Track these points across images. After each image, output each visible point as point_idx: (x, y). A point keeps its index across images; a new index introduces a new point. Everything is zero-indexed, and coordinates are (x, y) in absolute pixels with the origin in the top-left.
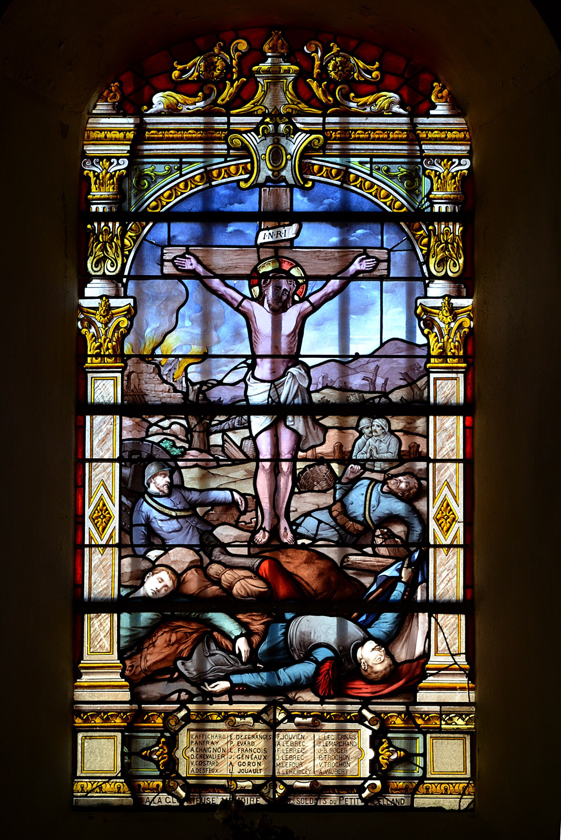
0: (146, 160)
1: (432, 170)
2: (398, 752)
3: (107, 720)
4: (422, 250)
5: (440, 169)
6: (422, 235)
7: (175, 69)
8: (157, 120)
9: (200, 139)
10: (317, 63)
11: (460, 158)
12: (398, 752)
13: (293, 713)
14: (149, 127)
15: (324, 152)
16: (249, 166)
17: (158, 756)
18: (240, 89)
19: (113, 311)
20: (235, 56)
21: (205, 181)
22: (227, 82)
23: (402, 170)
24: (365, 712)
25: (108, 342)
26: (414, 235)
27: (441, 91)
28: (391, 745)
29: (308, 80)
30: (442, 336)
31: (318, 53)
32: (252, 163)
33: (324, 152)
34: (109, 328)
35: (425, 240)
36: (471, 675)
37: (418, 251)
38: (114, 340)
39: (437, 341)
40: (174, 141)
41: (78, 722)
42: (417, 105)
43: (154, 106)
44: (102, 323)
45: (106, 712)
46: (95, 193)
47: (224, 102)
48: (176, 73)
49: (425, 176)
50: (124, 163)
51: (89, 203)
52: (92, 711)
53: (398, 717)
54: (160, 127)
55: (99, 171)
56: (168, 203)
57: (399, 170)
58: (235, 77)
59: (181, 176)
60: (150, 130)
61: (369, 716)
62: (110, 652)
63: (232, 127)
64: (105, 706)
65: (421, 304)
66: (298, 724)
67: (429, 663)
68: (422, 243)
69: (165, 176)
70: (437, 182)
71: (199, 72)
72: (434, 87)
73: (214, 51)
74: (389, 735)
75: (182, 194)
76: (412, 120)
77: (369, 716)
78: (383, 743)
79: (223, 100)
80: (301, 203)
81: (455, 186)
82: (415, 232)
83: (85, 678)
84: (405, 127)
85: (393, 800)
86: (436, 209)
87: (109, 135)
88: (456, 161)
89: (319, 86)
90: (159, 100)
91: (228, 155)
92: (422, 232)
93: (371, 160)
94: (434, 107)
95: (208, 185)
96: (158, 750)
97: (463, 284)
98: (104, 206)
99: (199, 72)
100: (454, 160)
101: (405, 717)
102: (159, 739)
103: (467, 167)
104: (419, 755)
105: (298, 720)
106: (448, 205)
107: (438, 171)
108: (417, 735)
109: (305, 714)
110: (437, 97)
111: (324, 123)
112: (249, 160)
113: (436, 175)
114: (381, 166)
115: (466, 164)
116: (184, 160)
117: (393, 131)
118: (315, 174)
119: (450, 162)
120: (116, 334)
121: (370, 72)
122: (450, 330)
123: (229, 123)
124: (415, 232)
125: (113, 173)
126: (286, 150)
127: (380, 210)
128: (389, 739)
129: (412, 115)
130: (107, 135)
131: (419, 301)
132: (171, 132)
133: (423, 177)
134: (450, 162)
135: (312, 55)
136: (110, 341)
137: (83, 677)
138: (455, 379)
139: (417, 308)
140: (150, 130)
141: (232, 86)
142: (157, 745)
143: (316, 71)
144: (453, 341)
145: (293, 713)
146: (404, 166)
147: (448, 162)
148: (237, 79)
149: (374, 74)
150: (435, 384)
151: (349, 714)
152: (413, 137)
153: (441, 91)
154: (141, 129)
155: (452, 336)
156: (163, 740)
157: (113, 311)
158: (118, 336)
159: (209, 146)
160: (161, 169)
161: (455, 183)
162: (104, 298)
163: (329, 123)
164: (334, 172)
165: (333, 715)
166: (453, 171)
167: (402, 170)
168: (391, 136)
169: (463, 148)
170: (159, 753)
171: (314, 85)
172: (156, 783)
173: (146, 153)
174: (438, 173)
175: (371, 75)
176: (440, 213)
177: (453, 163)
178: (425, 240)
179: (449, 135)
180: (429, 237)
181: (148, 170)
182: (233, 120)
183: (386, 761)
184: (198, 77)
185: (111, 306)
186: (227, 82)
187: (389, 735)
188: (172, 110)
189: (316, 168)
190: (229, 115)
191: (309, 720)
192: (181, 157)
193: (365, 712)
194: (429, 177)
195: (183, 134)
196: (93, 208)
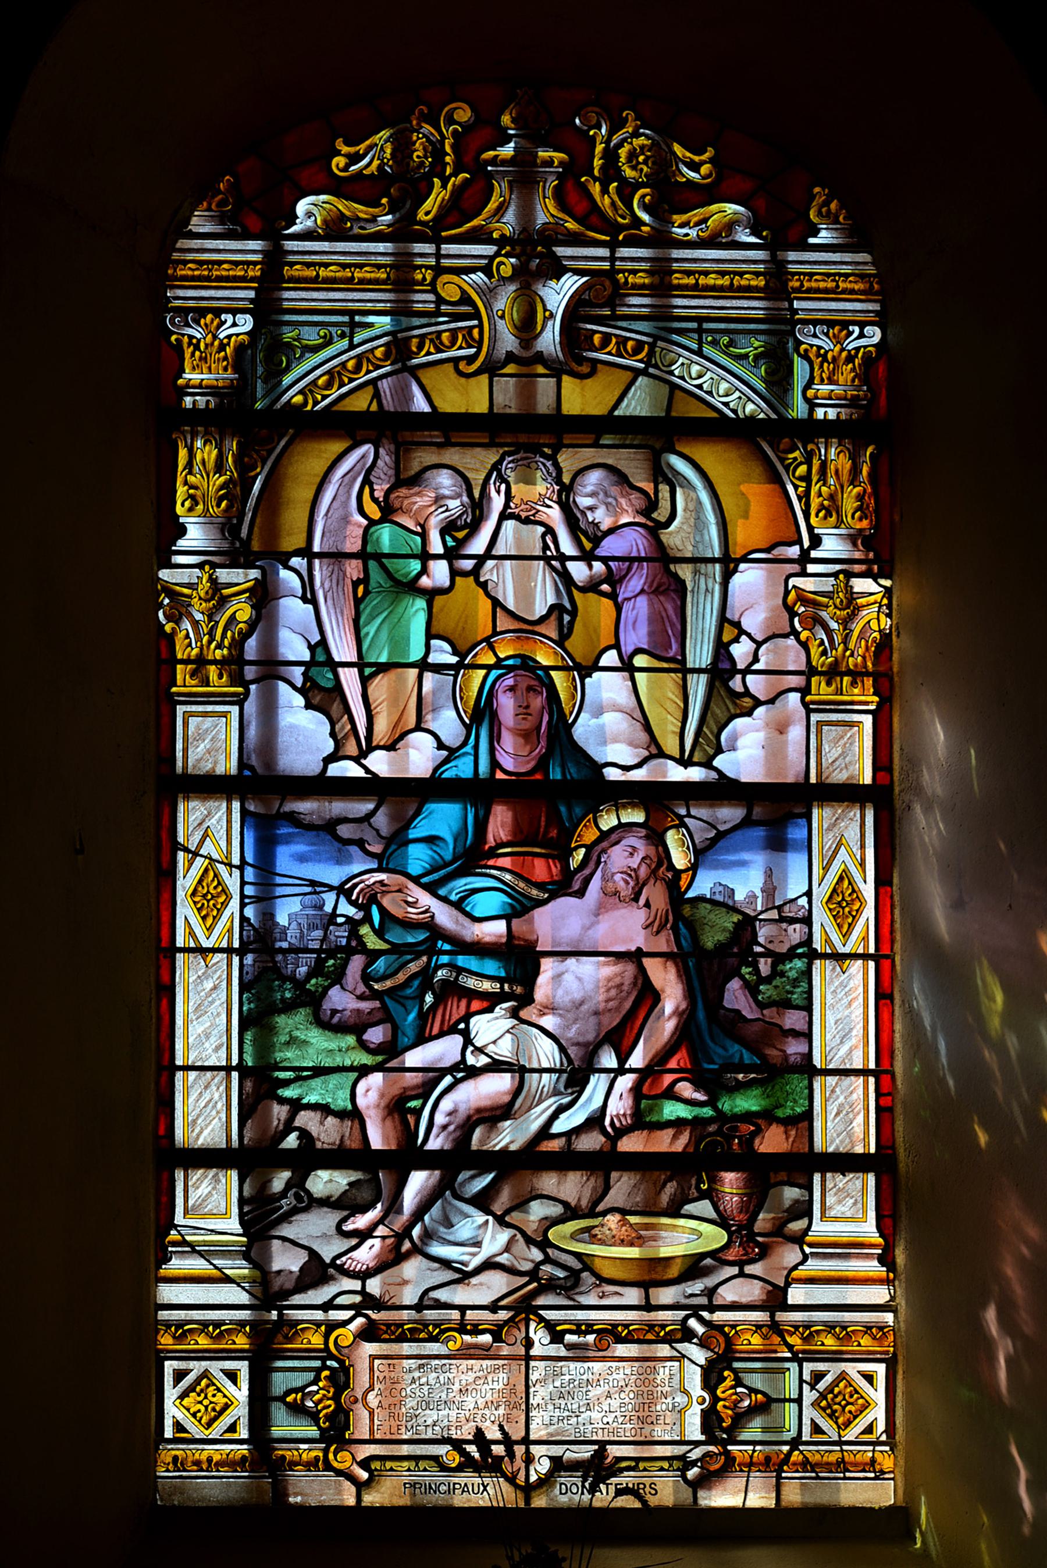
0: (287, 318)
1: (812, 346)
2: (753, 1395)
3: (179, 1339)
4: (796, 487)
5: (826, 343)
6: (795, 459)
7: (338, 153)
8: (304, 246)
9: (384, 282)
10: (599, 148)
11: (862, 325)
12: (753, 1395)
13: (558, 1328)
14: (291, 258)
15: (613, 311)
16: (476, 332)
17: (317, 1404)
18: (457, 191)
19: (226, 592)
20: (448, 131)
21: (392, 358)
22: (435, 180)
23: (757, 344)
24: (693, 1323)
25: (216, 648)
26: (782, 460)
27: (826, 203)
28: (739, 1383)
29: (583, 179)
30: (833, 647)
31: (600, 130)
32: (481, 326)
33: (613, 311)
34: (217, 623)
35: (802, 470)
36: (886, 1259)
37: (790, 488)
38: (226, 643)
39: (824, 653)
40: (331, 283)
41: (166, 1340)
42: (783, 230)
43: (298, 221)
44: (203, 613)
45: (217, 1324)
46: (191, 376)
47: (430, 217)
48: (339, 161)
49: (799, 355)
50: (246, 323)
51: (182, 392)
52: (232, 1322)
53: (756, 1332)
54: (308, 258)
55: (199, 336)
56: (324, 397)
57: (754, 346)
58: (448, 171)
59: (352, 347)
60: (292, 264)
61: (700, 1329)
62: (225, 1215)
63: (446, 262)
64: (847, 1316)
65: (794, 587)
66: (570, 1347)
67: (810, 1233)
68: (797, 474)
69: (315, 349)
70: (193, 354)
71: (382, 161)
72: (815, 196)
73: (411, 123)
74: (736, 1365)
75: (351, 380)
76: (773, 255)
77: (700, 1329)
78: (725, 1379)
79: (427, 213)
80: (579, 398)
81: (225, 363)
82: (783, 455)
83: (175, 1262)
84: (761, 267)
85: (466, 1485)
86: (820, 413)
87: (702, 281)
88: (229, 319)
89: (605, 191)
90: (309, 210)
91: (438, 313)
92: (796, 454)
93: (700, 325)
94: (815, 233)
95: (399, 366)
96: (317, 1392)
97: (878, 551)
98: (839, 410)
99: (382, 161)
100: (851, 328)
101: (214, 1331)
102: (318, 1371)
103: (876, 340)
104: (790, 1400)
105: (569, 1338)
106: (843, 410)
107: (822, 348)
108: (787, 1365)
109: (583, 1327)
110: (819, 214)
111: (612, 259)
112: (476, 322)
113: (818, 355)
114: (718, 337)
115: (874, 334)
116: (705, 326)
117: (811, 275)
118: (596, 350)
119: (845, 332)
120: (229, 634)
121: (695, 167)
122: (847, 634)
123: (438, 256)
124: (783, 455)
125: (853, 352)
126: (544, 306)
127: (715, 415)
128: (735, 1371)
129: (775, 245)
130: (700, 282)
131: (792, 582)
132: (225, 266)
133: (796, 356)
134: (845, 332)
135: (591, 133)
136: (219, 646)
137: (173, 1261)
138: (224, 715)
139: (787, 593)
140: (292, 264)
141: (444, 186)
142: (315, 1382)
143: (597, 163)
144: (852, 655)
145: (558, 1328)
146: (762, 337)
147: (841, 331)
148: (455, 174)
149: (705, 169)
150: (186, 724)
151: (663, 1327)
152: (777, 284)
153: (826, 203)
154: (275, 261)
155: (851, 646)
156: (326, 1373)
157: (226, 592)
158: (233, 637)
159: (402, 296)
160: (311, 336)
161: (853, 370)
162: (207, 568)
163: (623, 259)
164: (630, 344)
165: (408, 1329)
166: (850, 347)
167: (757, 344)
168: (806, 284)
169: (870, 306)
170: (317, 1397)
171: (596, 189)
172: (313, 1454)
173: (286, 305)
174: (822, 351)
175: (698, 171)
176: (825, 420)
177: (851, 333)
178: (802, 470)
179: (323, 273)
180: (809, 463)
181: (289, 335)
182: (446, 248)
183: (730, 1412)
184: (380, 168)
185: (855, 590)
186: (435, 180)
187: (736, 1365)
188: (335, 229)
189: (597, 338)
190: (438, 241)
191: (591, 1338)
192: (352, 313)
193: (693, 1323)
194: (805, 357)
195: (210, 270)
196: (188, 401)
